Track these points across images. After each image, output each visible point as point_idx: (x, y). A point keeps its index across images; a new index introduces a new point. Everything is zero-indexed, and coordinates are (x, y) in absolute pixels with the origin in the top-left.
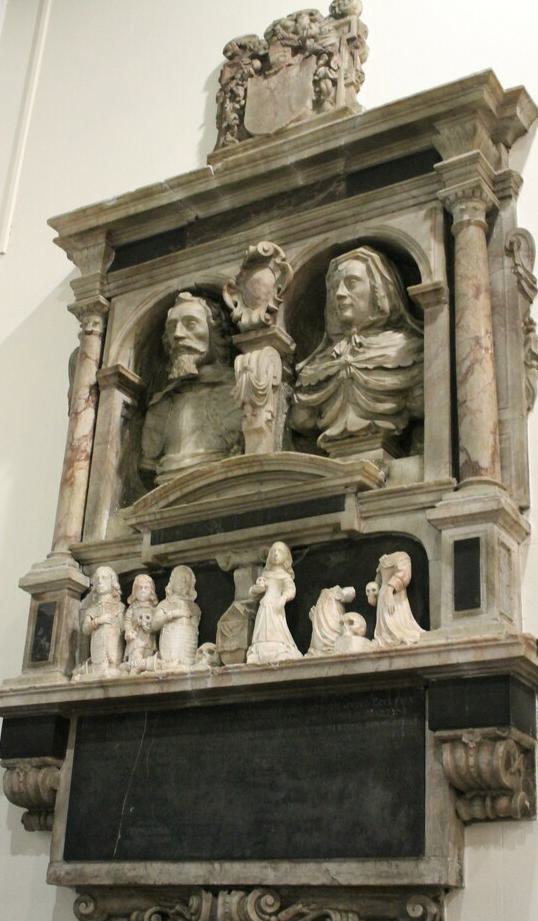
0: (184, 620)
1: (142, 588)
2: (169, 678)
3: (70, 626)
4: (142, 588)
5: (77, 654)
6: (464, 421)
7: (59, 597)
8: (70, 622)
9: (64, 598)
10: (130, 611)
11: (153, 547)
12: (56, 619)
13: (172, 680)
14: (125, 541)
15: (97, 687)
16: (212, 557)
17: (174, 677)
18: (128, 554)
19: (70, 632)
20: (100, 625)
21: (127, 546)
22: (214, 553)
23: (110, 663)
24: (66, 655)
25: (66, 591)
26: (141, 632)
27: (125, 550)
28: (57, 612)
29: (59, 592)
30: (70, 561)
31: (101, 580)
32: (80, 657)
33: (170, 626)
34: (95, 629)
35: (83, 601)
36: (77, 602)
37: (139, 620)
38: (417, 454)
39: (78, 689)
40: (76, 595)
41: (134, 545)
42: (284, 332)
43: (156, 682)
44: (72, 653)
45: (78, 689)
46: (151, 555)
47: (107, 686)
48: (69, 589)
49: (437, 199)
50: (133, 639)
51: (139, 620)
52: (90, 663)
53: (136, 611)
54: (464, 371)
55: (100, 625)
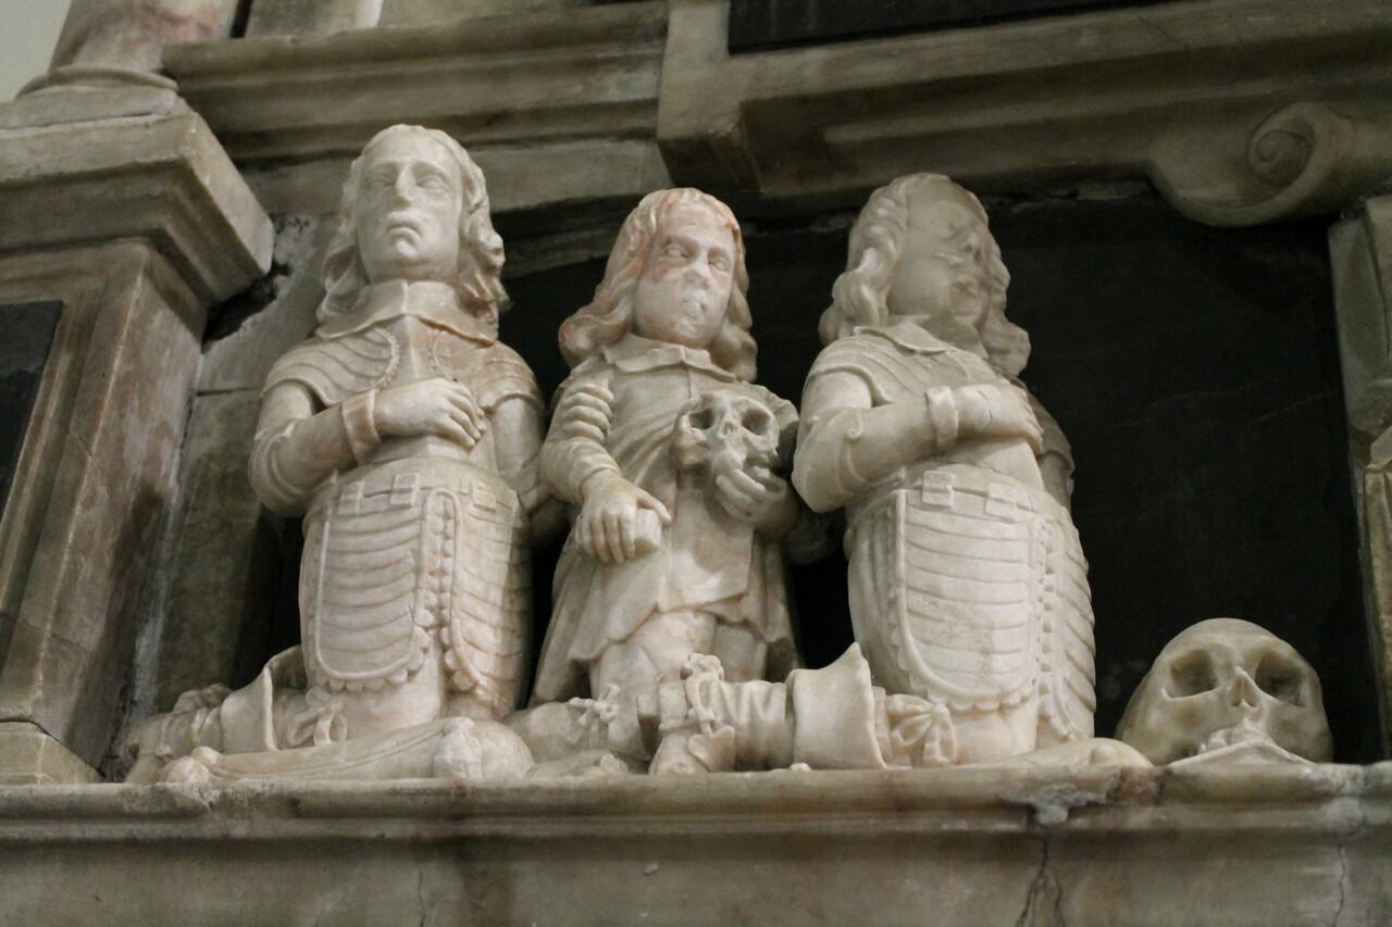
0: (1023, 453)
1: (690, 252)
2: (1140, 818)
3: (136, 468)
4: (690, 252)
5: (148, 645)
6: (971, 354)
7: (91, 284)
8: (138, 444)
9: (124, 283)
10: (589, 393)
11: (747, 65)
12: (49, 403)
13: (1166, 836)
14: (538, 41)
15: (419, 849)
16: (1126, 153)
17: (1184, 817)
18: (538, 114)
19: (129, 494)
20: (392, 439)
21: (538, 70)
22: (1142, 123)
23: (454, 692)
24: (89, 632)
25: (141, 251)
26: (694, 517)
27: (524, 94)
28: (63, 362)
29: (84, 258)
30: (169, 99)
31: (405, 181)
32: (168, 655)
33: (949, 478)
34: (350, 465)
35: (220, 347)
36: (185, 337)
37: (692, 435)
38: (1356, 216)
39: (227, 850)
40: (188, 296)
41: (588, 66)
42: (119, 526)
43: (1006, 850)
44: (122, 629)
45: (227, 850)
46: (732, 103)
47: (501, 846)
48: (160, 242)
49: (646, 135)
50: (643, 550)
51: (692, 435)
52: (294, 683)
53: (642, 391)
54: (659, 448)
55: (392, 439)
